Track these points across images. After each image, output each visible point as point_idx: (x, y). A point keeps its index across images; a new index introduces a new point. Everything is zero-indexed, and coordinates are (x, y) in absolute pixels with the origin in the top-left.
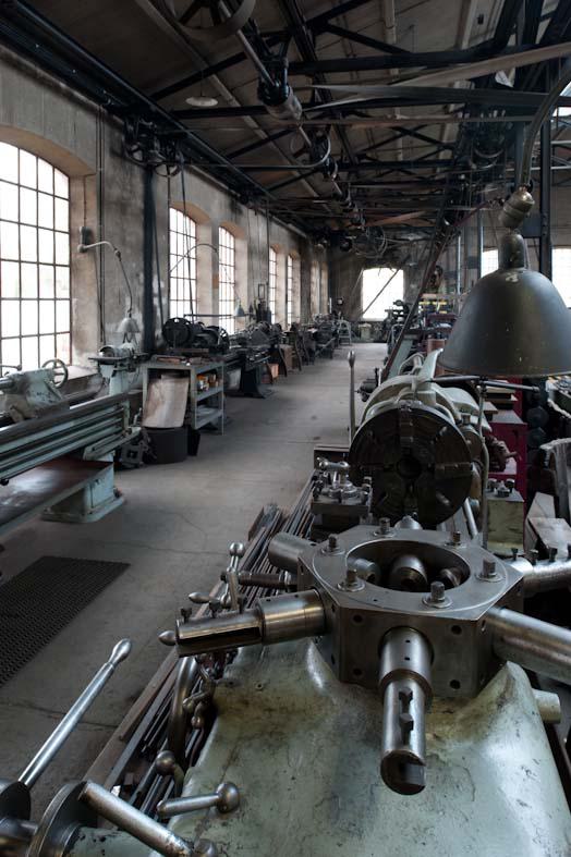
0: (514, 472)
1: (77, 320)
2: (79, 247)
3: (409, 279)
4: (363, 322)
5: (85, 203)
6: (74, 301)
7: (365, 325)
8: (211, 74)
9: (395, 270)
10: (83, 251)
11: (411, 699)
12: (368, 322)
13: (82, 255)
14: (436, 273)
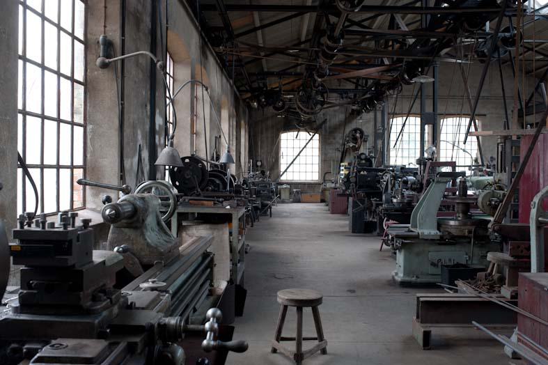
1: (93, 152)
2: (99, 61)
4: (282, 184)
5: (106, 7)
6: (89, 127)
7: (284, 186)
10: (104, 66)
12: (287, 184)
13: (101, 71)
14: (358, 135)
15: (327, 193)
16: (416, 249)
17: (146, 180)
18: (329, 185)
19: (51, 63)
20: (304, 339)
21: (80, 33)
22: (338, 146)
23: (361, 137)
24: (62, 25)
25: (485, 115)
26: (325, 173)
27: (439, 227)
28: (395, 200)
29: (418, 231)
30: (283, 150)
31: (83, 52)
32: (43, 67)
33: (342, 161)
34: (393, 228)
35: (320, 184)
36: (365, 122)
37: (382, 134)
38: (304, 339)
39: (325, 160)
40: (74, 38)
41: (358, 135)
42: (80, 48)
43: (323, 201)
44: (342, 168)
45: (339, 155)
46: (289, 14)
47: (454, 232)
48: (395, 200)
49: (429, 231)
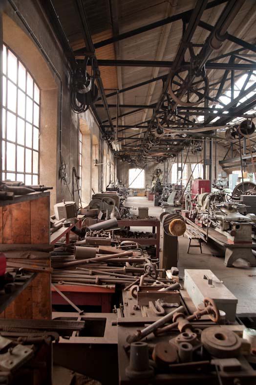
2: (95, 164)
3: (146, 173)
4: (129, 189)
10: (96, 165)
14: (159, 171)
15: (147, 193)
18: (148, 190)
19: (21, 141)
20: (16, 180)
21: (37, 124)
22: (151, 174)
26: (146, 185)
31: (14, 56)
32: (16, 144)
34: (163, 203)
36: (161, 166)
37: (167, 172)
38: (16, 180)
39: (147, 180)
40: (33, 126)
41: (159, 171)
42: (36, 131)
43: (145, 196)
45: (152, 178)
46: (133, 137)
47: (178, 204)
49: (172, 204)
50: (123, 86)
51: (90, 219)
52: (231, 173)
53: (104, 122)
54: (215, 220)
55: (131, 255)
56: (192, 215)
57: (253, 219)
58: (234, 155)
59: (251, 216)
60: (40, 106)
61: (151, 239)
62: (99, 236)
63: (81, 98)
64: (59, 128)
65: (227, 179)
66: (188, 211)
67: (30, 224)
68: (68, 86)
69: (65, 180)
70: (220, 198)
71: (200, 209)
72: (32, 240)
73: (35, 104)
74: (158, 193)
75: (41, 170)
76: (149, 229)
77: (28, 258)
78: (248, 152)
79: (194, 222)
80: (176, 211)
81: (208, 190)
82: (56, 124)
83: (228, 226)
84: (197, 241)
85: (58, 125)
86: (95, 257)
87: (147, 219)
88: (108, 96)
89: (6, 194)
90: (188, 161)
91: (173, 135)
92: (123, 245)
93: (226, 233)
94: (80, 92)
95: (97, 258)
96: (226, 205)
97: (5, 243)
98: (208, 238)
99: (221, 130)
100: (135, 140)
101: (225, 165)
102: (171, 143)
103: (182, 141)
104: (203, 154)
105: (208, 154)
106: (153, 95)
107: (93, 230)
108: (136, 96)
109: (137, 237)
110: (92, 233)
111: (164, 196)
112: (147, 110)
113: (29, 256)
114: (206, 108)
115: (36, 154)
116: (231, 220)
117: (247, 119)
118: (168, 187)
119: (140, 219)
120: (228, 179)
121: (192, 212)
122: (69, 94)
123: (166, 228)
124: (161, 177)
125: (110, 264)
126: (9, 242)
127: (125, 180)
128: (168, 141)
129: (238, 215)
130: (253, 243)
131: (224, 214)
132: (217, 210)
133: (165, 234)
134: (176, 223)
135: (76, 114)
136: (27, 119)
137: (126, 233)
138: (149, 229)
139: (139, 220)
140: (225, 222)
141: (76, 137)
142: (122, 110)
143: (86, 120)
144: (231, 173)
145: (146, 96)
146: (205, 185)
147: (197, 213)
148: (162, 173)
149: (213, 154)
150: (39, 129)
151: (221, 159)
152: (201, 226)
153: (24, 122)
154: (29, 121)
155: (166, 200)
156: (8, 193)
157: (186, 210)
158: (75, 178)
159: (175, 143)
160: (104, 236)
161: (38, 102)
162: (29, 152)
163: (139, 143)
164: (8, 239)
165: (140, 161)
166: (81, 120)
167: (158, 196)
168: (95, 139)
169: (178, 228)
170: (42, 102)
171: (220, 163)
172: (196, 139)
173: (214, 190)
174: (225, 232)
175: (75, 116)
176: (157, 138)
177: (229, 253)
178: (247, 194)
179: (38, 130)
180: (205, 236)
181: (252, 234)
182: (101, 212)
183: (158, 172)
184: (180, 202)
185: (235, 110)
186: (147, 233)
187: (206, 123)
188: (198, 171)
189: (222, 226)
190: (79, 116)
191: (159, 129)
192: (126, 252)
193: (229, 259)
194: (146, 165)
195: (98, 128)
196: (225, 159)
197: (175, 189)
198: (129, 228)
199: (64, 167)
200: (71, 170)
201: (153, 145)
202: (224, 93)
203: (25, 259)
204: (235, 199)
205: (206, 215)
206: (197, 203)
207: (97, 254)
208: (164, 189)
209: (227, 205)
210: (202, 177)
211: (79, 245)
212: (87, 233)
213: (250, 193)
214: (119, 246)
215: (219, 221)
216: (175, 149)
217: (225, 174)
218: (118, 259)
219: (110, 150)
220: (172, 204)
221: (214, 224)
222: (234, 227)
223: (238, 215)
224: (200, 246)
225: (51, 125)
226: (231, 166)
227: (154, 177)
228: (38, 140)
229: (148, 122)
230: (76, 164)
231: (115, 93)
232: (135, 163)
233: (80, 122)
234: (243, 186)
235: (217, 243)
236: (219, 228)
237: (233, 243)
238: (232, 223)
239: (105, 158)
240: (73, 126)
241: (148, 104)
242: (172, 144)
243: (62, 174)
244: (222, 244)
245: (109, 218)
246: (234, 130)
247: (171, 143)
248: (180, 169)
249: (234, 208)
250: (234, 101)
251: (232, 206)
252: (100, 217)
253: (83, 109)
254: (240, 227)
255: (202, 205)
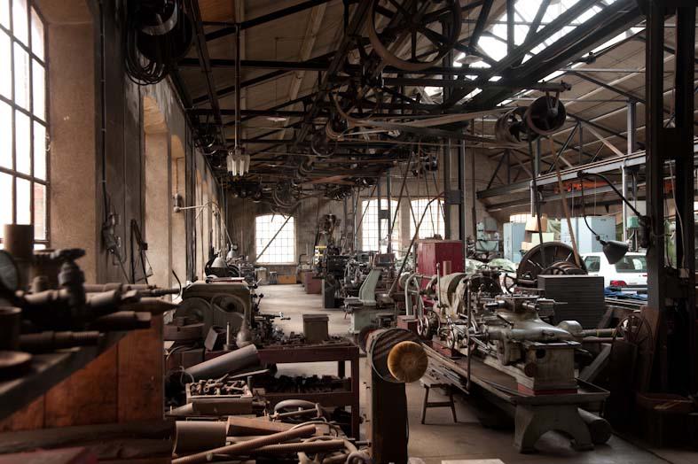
0: (335, 364)
2: (175, 208)
3: (300, 225)
4: (258, 267)
7: (261, 269)
8: (662, 95)
9: (271, 216)
10: (178, 211)
11: (589, 364)
12: (264, 266)
15: (303, 275)
16: (363, 312)
17: (603, 323)
18: (305, 267)
21: (40, 112)
22: (314, 230)
23: (334, 221)
24: (17, 102)
25: (289, 319)
26: (300, 256)
27: (376, 297)
28: (352, 282)
29: (362, 301)
30: (258, 235)
33: (316, 245)
35: (295, 266)
36: (335, 208)
37: (352, 224)
39: (300, 242)
40: (33, 118)
41: (331, 220)
42: (40, 131)
43: (299, 282)
44: (316, 251)
47: (385, 301)
48: (352, 282)
49: (370, 301)
50: (246, 12)
51: (185, 351)
52: (508, 221)
53: (196, 101)
54: (487, 339)
55: (309, 434)
56: (425, 327)
57: (575, 333)
58: (512, 177)
59: (571, 327)
60: (45, 65)
61: (337, 391)
62: (222, 393)
63: (148, 45)
64: (100, 123)
65: (497, 234)
66: (413, 317)
67: (117, 376)
68: (116, 16)
69: (116, 253)
70: (489, 282)
71: (444, 313)
72: (121, 413)
73: (34, 61)
74: (332, 274)
75: (54, 230)
76: (328, 368)
77: (119, 456)
78: (546, 167)
79: (430, 345)
80: (382, 318)
81: (458, 266)
82: (93, 113)
83: (519, 351)
84: (442, 392)
85: (96, 117)
86: (224, 445)
87: (325, 343)
88: (210, 37)
89: (135, 316)
90: (404, 193)
91: (365, 133)
92: (280, 411)
93: (511, 370)
94: (149, 31)
95: (228, 447)
96: (510, 301)
97: (50, 427)
98: (473, 383)
99: (487, 119)
100: (267, 145)
101: (492, 200)
102: (361, 150)
103: (388, 146)
104: (442, 177)
105: (453, 175)
106: (318, 35)
107: (198, 377)
108: (277, 38)
109: (304, 388)
110: (203, 384)
111: (348, 282)
112: (301, 73)
113: (120, 451)
114: (447, 70)
115: (41, 190)
116: (523, 338)
117: (547, 94)
118: (356, 258)
119: (309, 344)
120: (502, 234)
121: (424, 321)
122: (118, 35)
123: (379, 365)
124: (336, 235)
125: (259, 458)
126: (60, 422)
127: (247, 244)
128: (356, 147)
129: (539, 326)
130: (580, 392)
131: (505, 323)
132: (487, 314)
133: (375, 378)
134: (403, 350)
135: (136, 86)
136: (17, 103)
137: (279, 386)
138: (328, 368)
139: (306, 346)
140: (510, 342)
141: (137, 142)
142: (243, 71)
143: (155, 103)
144: (508, 221)
145: (303, 38)
146: (449, 253)
147: (436, 322)
148: (338, 225)
149: (466, 174)
150: (47, 124)
151: (481, 187)
152: (450, 355)
153: (28, 118)
154: (23, 106)
155: (355, 291)
156: (139, 314)
157: (408, 317)
158: (136, 246)
159: (372, 151)
160: (233, 392)
161: (41, 56)
162: (24, 185)
163: (281, 151)
164: (57, 416)
165: (285, 195)
166: (145, 98)
167: (332, 282)
168: (177, 141)
169: (410, 363)
170: (51, 55)
171: (481, 196)
172: (426, 140)
173: (472, 265)
174: (511, 368)
175: (134, 88)
176: (331, 141)
177: (523, 417)
178: (552, 274)
179: (43, 129)
180: (463, 379)
181: (576, 368)
182: (211, 330)
183: (329, 223)
184: (393, 296)
185: (517, 71)
186: (327, 378)
187: (446, 106)
188: (430, 218)
189: (502, 353)
190: (142, 92)
191: (337, 119)
192: (293, 429)
193: (525, 435)
194: (300, 204)
195: (183, 118)
196: (492, 187)
197: (377, 265)
198: (274, 369)
199: (114, 221)
200: (128, 228)
201: (320, 158)
202: (486, 30)
203: (111, 459)
204: (524, 285)
205: (461, 327)
206: (436, 299)
207: (228, 438)
208: (348, 266)
209: (512, 302)
210: (442, 233)
211: (182, 418)
212: (188, 386)
213: (560, 270)
214: (276, 414)
215: (494, 341)
216: (372, 169)
217: (491, 223)
218: (279, 445)
219: (209, 172)
220: (370, 301)
221: (483, 347)
222: (533, 354)
223: (539, 326)
224: (451, 404)
225: (81, 113)
226: (507, 204)
227: (318, 236)
228: (44, 153)
229: (306, 100)
230: (138, 211)
231: (228, 29)
232: (273, 202)
233: (145, 105)
234: (543, 253)
235: (496, 396)
236: (495, 358)
237: (532, 394)
238: (527, 345)
239: (198, 191)
240: (130, 114)
241: (306, 57)
242: (363, 155)
243: (111, 239)
244: (507, 397)
245: (234, 347)
246: (515, 120)
247: (361, 150)
248: (384, 214)
249: (530, 309)
250: (515, 52)
251: (525, 304)
252: (210, 343)
253: (155, 75)
254: (547, 353)
255: (448, 303)
